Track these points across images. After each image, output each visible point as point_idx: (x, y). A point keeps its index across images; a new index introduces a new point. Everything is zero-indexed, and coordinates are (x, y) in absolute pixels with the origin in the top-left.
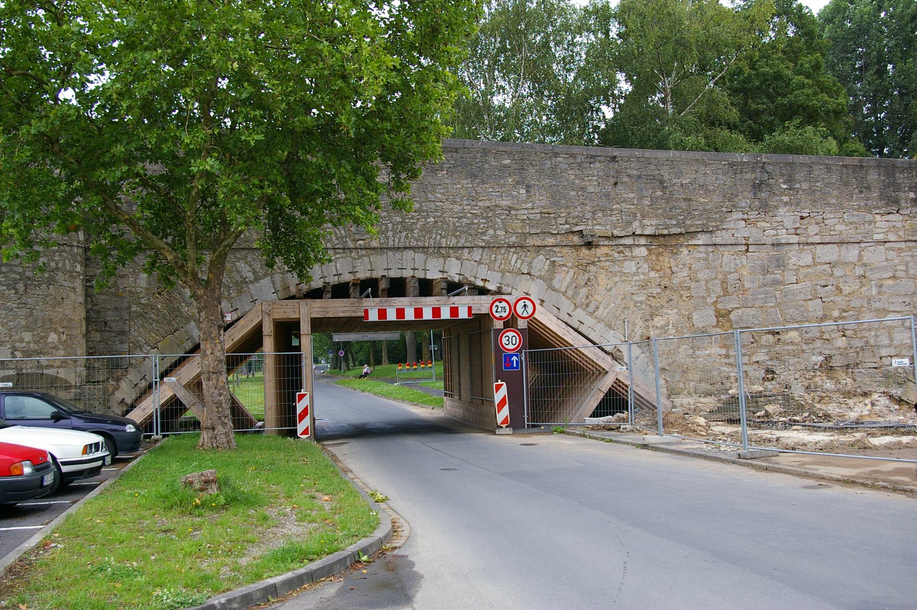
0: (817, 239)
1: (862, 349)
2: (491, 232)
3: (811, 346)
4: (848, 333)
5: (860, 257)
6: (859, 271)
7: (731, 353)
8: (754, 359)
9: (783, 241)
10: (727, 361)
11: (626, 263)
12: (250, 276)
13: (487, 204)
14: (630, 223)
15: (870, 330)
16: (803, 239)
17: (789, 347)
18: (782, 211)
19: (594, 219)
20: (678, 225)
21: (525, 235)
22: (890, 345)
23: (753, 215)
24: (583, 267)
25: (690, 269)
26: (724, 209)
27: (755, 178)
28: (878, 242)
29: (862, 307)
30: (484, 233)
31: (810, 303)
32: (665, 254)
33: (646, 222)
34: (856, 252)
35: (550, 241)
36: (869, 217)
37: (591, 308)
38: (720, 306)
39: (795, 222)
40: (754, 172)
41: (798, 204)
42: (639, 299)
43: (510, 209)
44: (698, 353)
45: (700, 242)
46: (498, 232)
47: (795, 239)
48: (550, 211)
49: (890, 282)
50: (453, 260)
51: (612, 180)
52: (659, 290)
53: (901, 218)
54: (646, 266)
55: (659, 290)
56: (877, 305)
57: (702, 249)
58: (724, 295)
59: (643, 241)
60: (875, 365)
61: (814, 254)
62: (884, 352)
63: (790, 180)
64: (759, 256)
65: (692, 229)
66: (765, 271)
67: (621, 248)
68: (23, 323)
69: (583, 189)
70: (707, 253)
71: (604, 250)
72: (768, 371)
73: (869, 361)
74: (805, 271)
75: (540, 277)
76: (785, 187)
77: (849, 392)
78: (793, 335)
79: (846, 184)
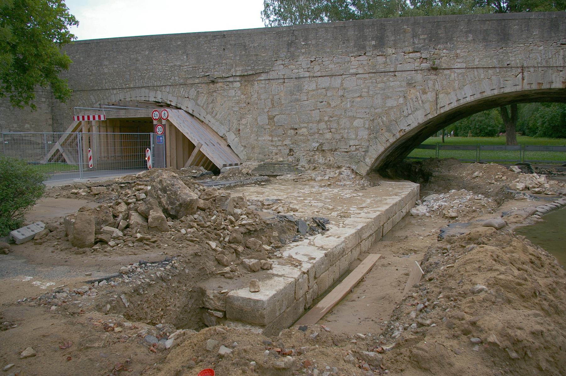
0: (319, 74)
1: (340, 140)
2: (173, 78)
3: (313, 137)
4: (332, 130)
5: (342, 84)
6: (341, 93)
7: (274, 140)
8: (285, 143)
9: (301, 76)
10: (272, 143)
11: (230, 91)
12: (94, 101)
13: (172, 64)
14: (230, 70)
15: (345, 129)
16: (312, 74)
17: (301, 137)
18: (301, 58)
19: (214, 69)
20: (251, 70)
21: (187, 79)
22: (355, 139)
23: (287, 62)
24: (210, 93)
25: (258, 93)
26: (273, 59)
27: (289, 40)
28: (353, 74)
29: (341, 115)
30: (170, 79)
31: (313, 112)
32: (249, 85)
33: (237, 69)
34: (339, 81)
35: (197, 81)
36: (348, 59)
37: (214, 115)
38: (270, 114)
39: (307, 64)
40: (288, 36)
41: (309, 53)
42: (235, 109)
43: (180, 66)
44: (259, 139)
45: (262, 78)
46: (176, 78)
47: (307, 74)
48: (197, 66)
49: (359, 99)
50: (159, 92)
51: (223, 47)
52: (245, 105)
53: (367, 58)
54: (239, 92)
55: (245, 105)
56: (350, 114)
57: (263, 82)
58: (272, 108)
59: (238, 79)
60: (346, 150)
61: (317, 83)
62: (352, 143)
63: (306, 40)
64: (290, 84)
65: (258, 71)
66: (292, 94)
67: (228, 83)
68: (13, 121)
69: (210, 53)
70: (265, 84)
71: (220, 84)
72: (291, 150)
73: (343, 147)
74: (311, 93)
75: (193, 99)
76: (303, 43)
77: (331, 166)
78: (304, 130)
79: (336, 39)
